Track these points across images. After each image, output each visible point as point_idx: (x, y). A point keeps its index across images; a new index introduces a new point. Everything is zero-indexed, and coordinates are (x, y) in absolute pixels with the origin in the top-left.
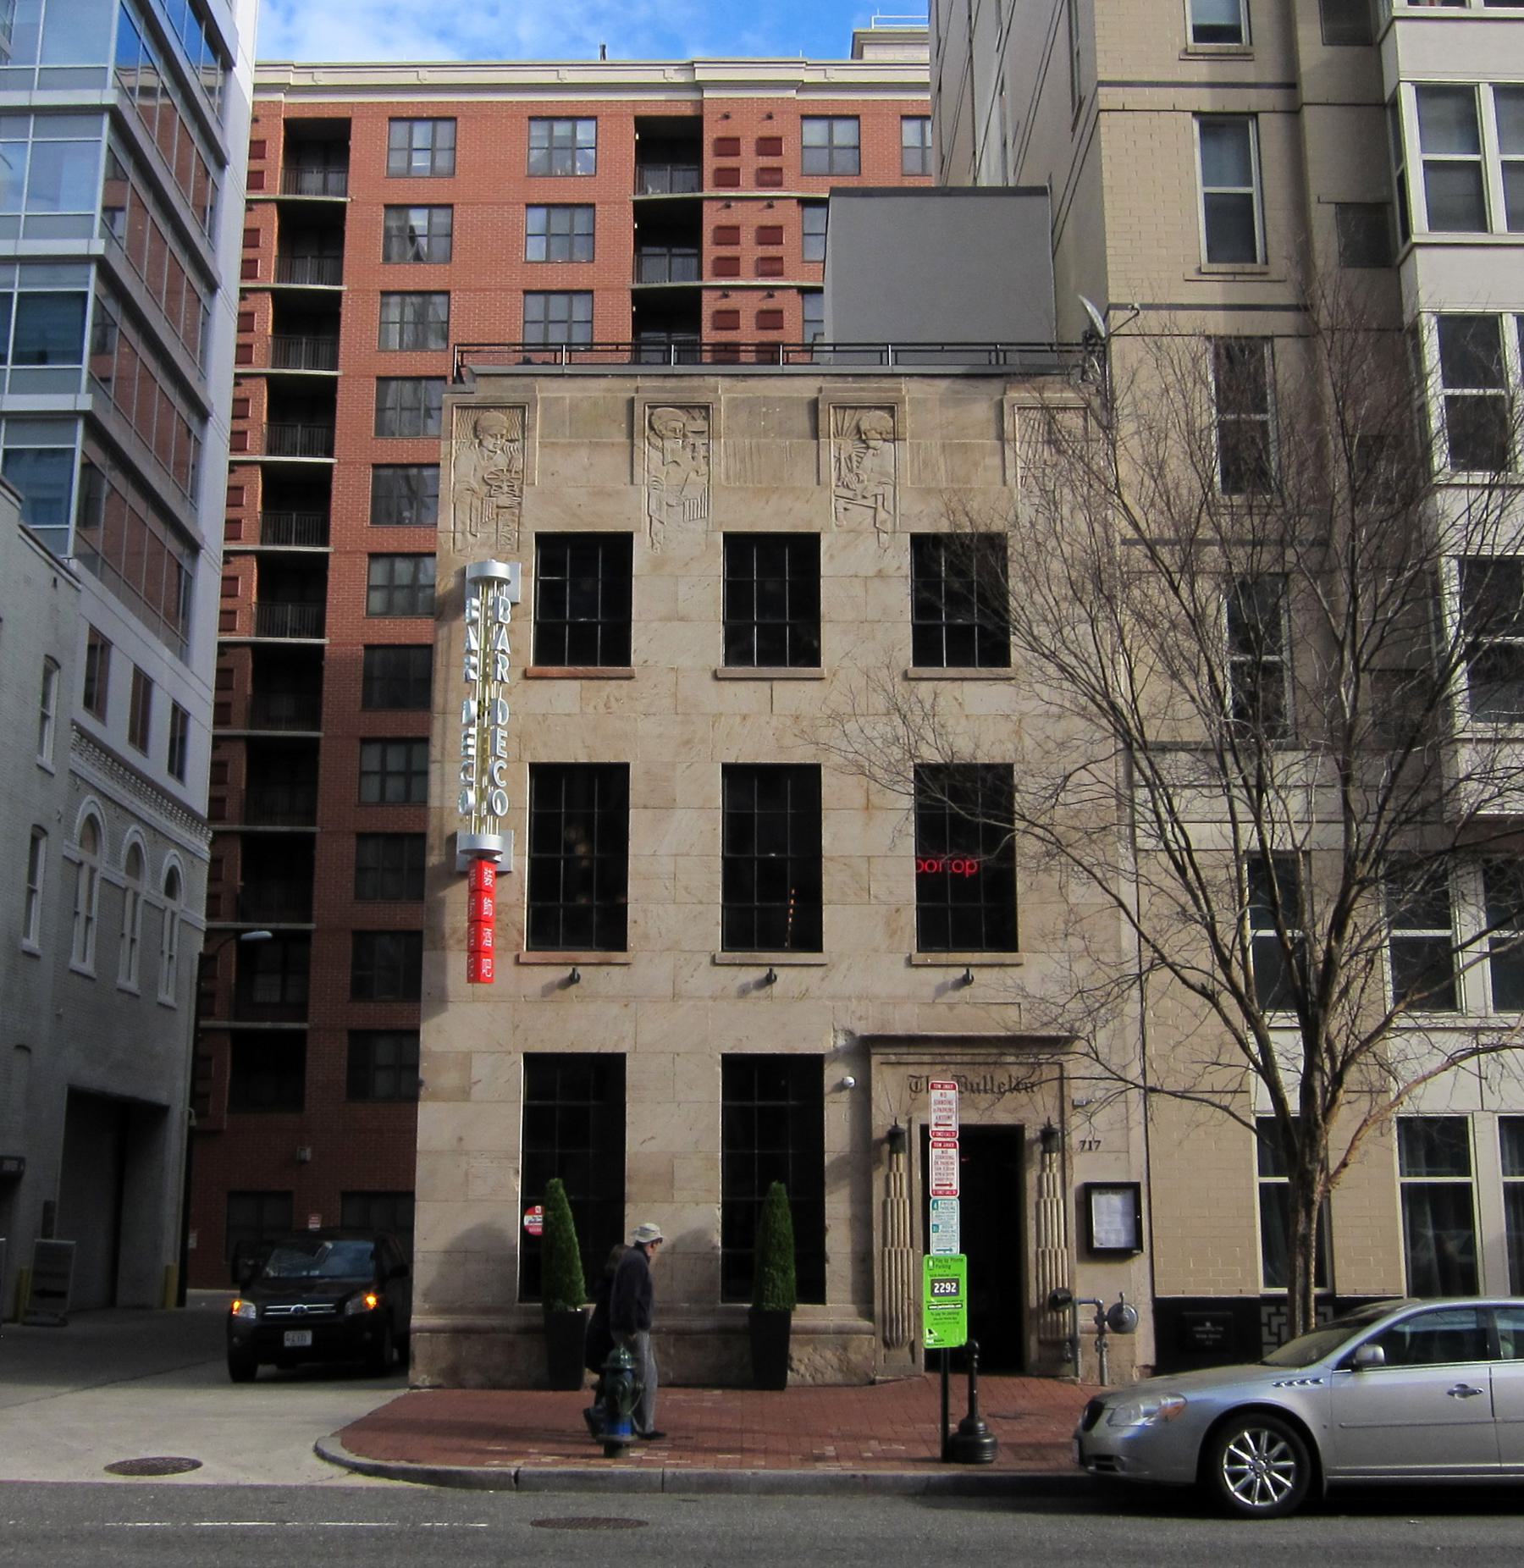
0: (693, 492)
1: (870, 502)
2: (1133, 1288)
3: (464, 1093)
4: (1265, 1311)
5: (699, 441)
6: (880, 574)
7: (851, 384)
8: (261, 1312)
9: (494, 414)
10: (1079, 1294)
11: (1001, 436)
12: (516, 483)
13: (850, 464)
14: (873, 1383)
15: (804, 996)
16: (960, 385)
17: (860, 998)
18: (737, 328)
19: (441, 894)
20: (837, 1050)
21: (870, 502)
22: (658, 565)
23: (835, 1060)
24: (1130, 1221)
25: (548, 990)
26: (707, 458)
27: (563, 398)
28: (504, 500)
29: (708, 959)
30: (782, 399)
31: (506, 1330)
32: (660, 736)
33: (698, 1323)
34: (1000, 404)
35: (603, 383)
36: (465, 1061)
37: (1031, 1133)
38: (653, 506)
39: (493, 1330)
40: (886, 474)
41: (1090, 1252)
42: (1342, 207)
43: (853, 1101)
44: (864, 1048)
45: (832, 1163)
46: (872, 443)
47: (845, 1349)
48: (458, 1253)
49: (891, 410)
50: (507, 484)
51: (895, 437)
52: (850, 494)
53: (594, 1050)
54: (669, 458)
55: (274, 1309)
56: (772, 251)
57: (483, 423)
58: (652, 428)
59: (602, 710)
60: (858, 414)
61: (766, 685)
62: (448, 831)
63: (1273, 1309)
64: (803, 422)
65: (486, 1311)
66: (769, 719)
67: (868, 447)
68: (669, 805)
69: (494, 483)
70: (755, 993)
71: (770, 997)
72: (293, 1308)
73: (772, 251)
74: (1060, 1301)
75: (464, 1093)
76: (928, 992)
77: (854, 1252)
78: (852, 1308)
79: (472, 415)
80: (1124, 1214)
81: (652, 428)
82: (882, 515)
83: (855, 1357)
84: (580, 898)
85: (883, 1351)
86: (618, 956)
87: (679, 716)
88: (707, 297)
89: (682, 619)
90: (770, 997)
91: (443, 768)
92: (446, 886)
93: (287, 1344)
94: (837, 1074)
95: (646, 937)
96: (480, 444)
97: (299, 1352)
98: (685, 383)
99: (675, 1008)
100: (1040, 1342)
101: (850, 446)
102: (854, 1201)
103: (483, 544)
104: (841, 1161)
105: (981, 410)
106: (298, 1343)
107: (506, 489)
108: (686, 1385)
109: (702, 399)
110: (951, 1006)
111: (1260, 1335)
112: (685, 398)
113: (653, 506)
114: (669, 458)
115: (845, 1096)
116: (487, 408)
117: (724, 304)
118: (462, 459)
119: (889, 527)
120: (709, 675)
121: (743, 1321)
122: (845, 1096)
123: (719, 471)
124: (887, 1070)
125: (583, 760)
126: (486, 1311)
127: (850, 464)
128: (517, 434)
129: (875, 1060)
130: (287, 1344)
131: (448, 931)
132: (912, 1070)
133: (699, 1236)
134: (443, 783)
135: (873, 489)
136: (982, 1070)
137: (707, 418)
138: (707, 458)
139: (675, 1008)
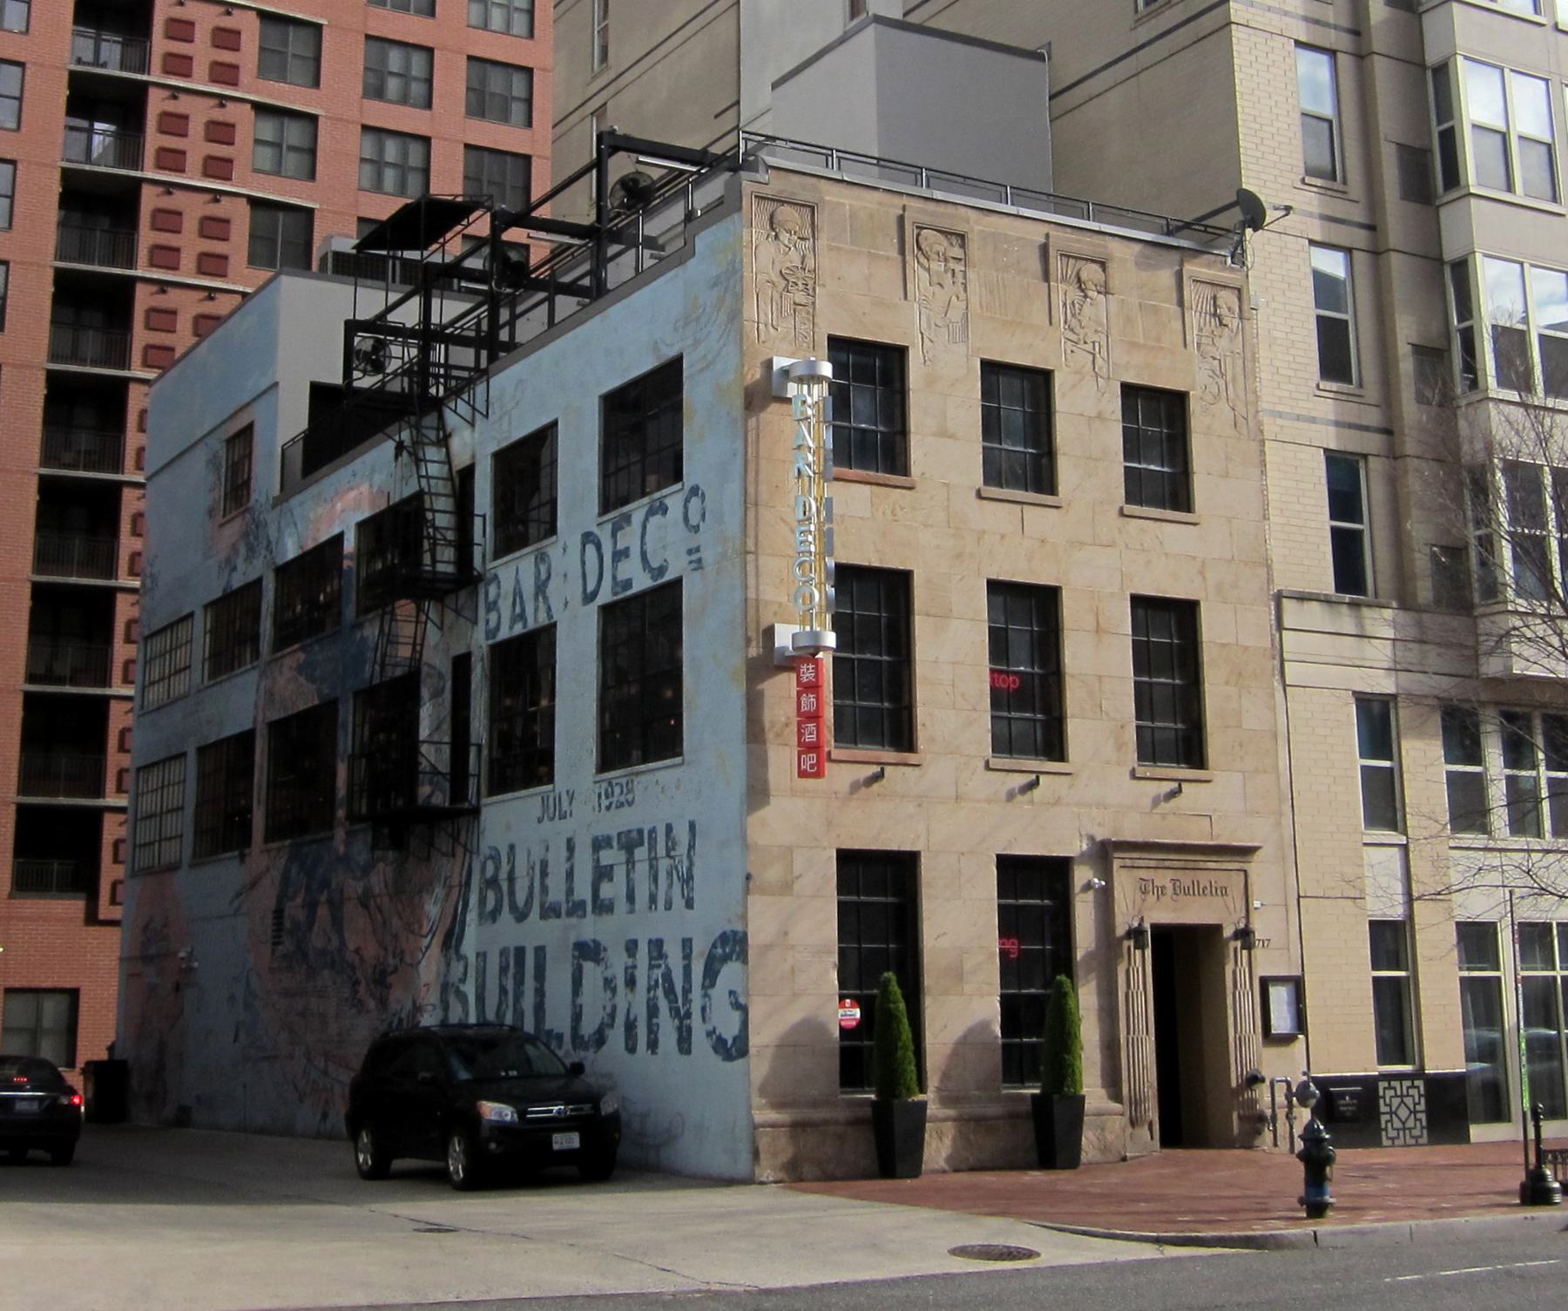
0: (956, 315)
1: (1089, 347)
2: (1283, 1068)
3: (786, 887)
4: (1382, 1085)
5: (959, 267)
6: (1100, 416)
7: (1075, 236)
8: (522, 1114)
9: (787, 209)
10: (1266, 1072)
11: (1181, 303)
12: (811, 283)
13: (1074, 311)
14: (1124, 1159)
15: (1057, 802)
16: (1149, 250)
17: (1098, 806)
18: (185, 135)
19: (760, 687)
20: (1083, 854)
21: (1089, 347)
22: (931, 381)
23: (1082, 863)
24: (1293, 1008)
25: (855, 787)
26: (965, 285)
27: (843, 204)
28: (800, 297)
29: (982, 764)
30: (1019, 239)
31: (837, 1122)
32: (938, 547)
33: (992, 1110)
34: (1179, 276)
35: (876, 195)
36: (788, 852)
37: (1228, 932)
38: (924, 325)
39: (826, 1122)
40: (1101, 324)
41: (1269, 1037)
42: (1401, 147)
43: (1096, 901)
44: (1104, 853)
45: (1083, 958)
46: (1090, 293)
47: (1103, 1129)
48: (957, 1030)
49: (1103, 265)
50: (801, 281)
51: (1106, 291)
52: (1074, 338)
53: (895, 848)
54: (935, 280)
55: (537, 1111)
56: (226, 57)
57: (778, 217)
58: (919, 248)
59: (890, 517)
60: (1080, 264)
61: (1018, 508)
62: (764, 624)
63: (1409, 1083)
64: (1035, 265)
65: (815, 1104)
66: (1023, 540)
67: (1086, 296)
68: (947, 615)
69: (792, 279)
70: (1019, 798)
71: (1032, 802)
72: (556, 1108)
73: (226, 57)
74: (1254, 1080)
75: (786, 887)
76: (1147, 802)
77: (1102, 1041)
78: (1102, 1092)
79: (770, 207)
80: (1289, 1004)
81: (919, 248)
82: (1099, 361)
83: (1110, 1137)
84: (876, 697)
85: (1129, 1130)
86: (911, 758)
87: (948, 530)
88: (154, 96)
89: (950, 437)
90: (1032, 802)
91: (757, 560)
92: (763, 681)
93: (556, 1147)
94: (1082, 875)
95: (932, 740)
96: (776, 237)
97: (567, 1155)
98: (941, 208)
99: (956, 809)
100: (1240, 1117)
101: (1074, 294)
102: (1100, 994)
103: (784, 338)
104: (1090, 956)
105: (1166, 277)
106: (565, 1146)
107: (801, 287)
108: (972, 1169)
109: (960, 228)
110: (1164, 816)
111: (1378, 1106)
112: (946, 224)
113: (924, 325)
114: (935, 280)
115: (1090, 895)
116: (783, 202)
117: (171, 106)
118: (761, 248)
119: (1104, 372)
120: (974, 494)
121: (1027, 1107)
122: (1090, 895)
123: (974, 299)
124: (1124, 872)
125: (876, 564)
126: (815, 1104)
127: (1074, 311)
128: (807, 233)
129: (1116, 864)
130: (556, 1147)
131: (767, 725)
132: (1143, 874)
133: (985, 1026)
134: (757, 575)
135: (1092, 337)
136: (1170, 874)
137: (963, 246)
138: (965, 285)
139: (956, 809)
